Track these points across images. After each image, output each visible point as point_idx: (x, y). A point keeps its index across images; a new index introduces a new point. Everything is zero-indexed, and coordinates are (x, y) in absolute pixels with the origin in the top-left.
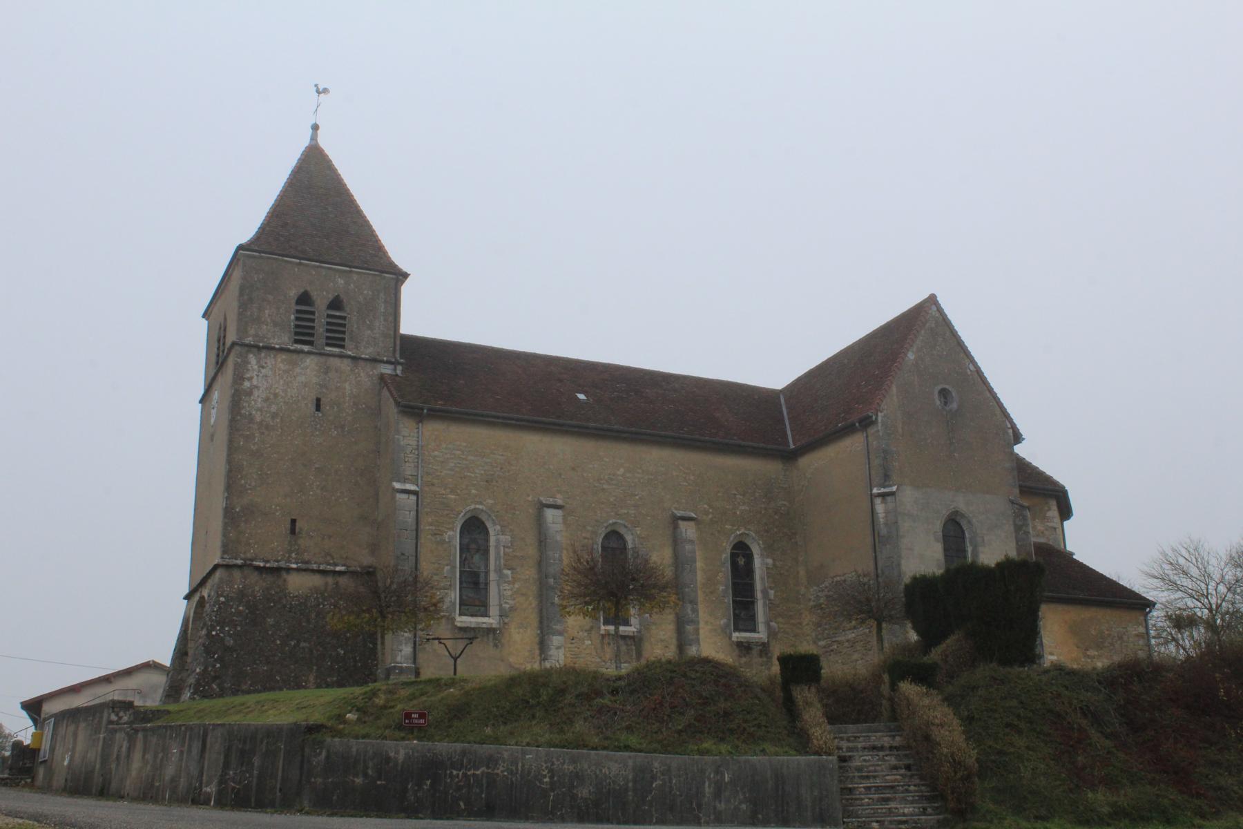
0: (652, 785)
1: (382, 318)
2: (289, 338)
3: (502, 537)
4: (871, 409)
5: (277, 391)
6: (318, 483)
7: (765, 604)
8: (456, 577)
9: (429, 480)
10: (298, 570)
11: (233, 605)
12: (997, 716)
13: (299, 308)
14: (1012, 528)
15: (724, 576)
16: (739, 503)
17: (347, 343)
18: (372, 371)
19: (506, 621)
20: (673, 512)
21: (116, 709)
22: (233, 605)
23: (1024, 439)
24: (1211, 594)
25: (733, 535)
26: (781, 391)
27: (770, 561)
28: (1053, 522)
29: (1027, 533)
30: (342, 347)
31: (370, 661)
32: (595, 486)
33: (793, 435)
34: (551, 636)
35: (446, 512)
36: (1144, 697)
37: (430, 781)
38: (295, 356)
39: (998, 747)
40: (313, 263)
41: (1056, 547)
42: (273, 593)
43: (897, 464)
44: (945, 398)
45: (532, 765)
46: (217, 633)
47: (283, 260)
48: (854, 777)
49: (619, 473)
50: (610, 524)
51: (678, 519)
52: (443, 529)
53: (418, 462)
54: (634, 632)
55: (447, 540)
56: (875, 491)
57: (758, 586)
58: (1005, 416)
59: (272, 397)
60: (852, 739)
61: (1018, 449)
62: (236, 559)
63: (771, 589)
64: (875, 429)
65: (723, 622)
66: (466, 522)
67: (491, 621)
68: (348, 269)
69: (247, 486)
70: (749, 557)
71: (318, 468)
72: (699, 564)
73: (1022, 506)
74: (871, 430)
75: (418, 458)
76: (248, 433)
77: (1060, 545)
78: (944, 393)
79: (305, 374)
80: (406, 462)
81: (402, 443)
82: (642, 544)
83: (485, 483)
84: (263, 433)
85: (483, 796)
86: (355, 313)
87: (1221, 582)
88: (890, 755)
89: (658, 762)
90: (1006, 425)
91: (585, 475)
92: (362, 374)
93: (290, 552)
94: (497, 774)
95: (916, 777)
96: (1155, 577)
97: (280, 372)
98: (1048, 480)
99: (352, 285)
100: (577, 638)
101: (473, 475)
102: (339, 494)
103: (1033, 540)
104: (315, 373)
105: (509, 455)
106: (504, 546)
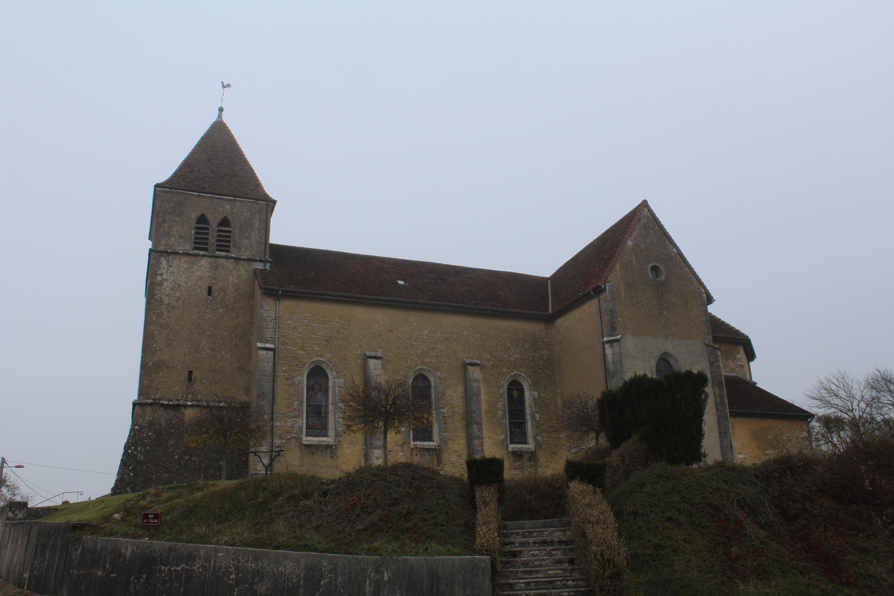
0: (320, 582)
2: (190, 246)
3: (337, 380)
5: (181, 282)
6: (208, 346)
7: (533, 424)
8: (303, 409)
11: (144, 432)
14: (708, 364)
15: (503, 405)
16: (513, 354)
17: (232, 249)
20: (464, 361)
21: (12, 509)
22: (144, 432)
23: (714, 300)
24: (856, 410)
26: (549, 278)
27: (536, 393)
28: (741, 361)
29: (719, 367)
30: (228, 251)
31: (243, 470)
35: (296, 363)
37: (145, 575)
38: (193, 258)
39: (656, 541)
41: (744, 378)
43: (621, 319)
44: (656, 272)
45: (221, 562)
46: (132, 452)
47: (187, 194)
48: (518, 572)
49: (423, 333)
50: (417, 370)
53: (275, 328)
54: (435, 446)
55: (296, 383)
56: (605, 339)
57: (528, 411)
58: (700, 284)
60: (527, 534)
61: (711, 309)
62: (148, 399)
63: (537, 413)
64: (605, 295)
66: (311, 370)
67: (329, 440)
68: (232, 198)
69: (157, 348)
70: (521, 391)
71: (209, 335)
72: (483, 397)
73: (715, 348)
74: (602, 296)
77: (746, 378)
78: (655, 269)
85: (182, 590)
87: (862, 400)
88: (557, 549)
89: (326, 561)
94: (194, 570)
95: (576, 572)
96: (816, 399)
98: (737, 332)
99: (236, 209)
101: (316, 337)
102: (223, 353)
103: (723, 374)
104: (207, 269)
105: (343, 322)
106: (338, 386)
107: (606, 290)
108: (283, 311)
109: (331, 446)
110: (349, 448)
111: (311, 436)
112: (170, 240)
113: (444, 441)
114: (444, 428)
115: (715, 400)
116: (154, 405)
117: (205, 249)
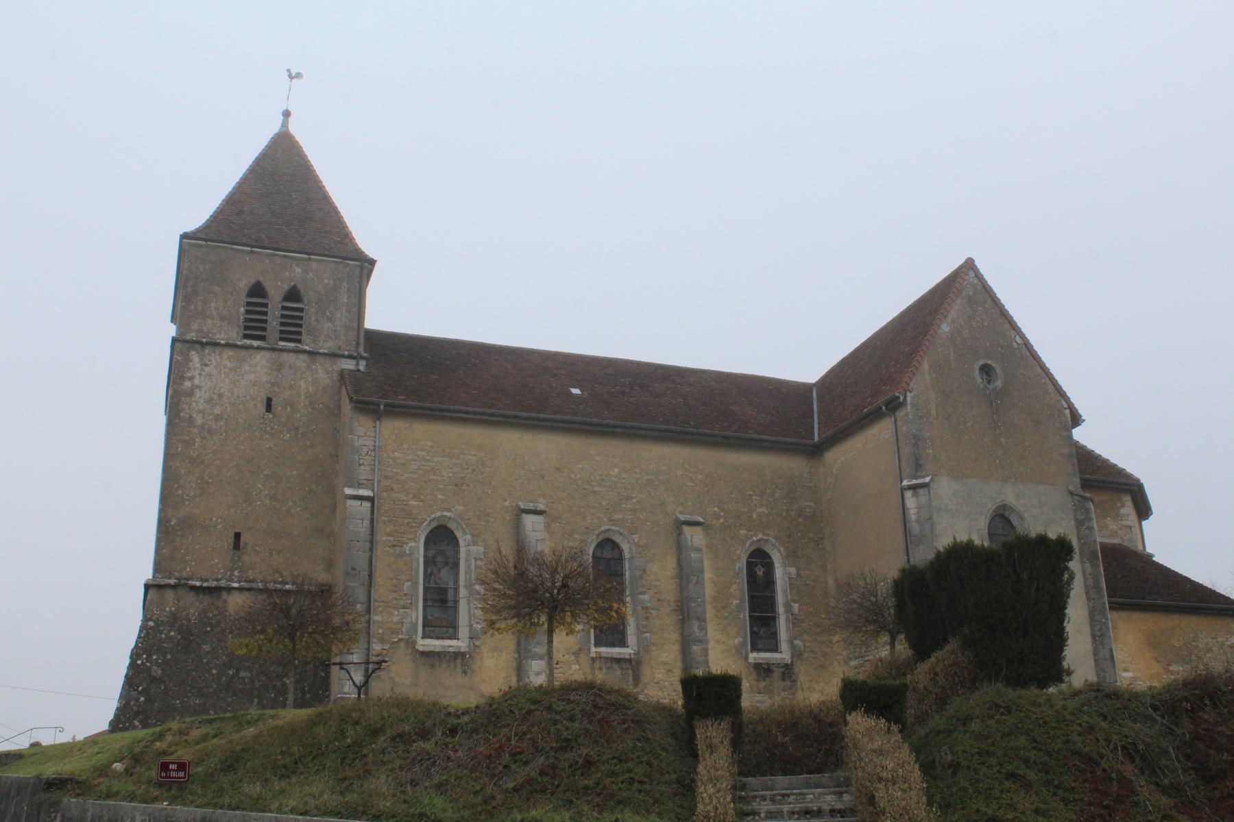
1: (344, 309)
2: (238, 333)
3: (473, 548)
4: (898, 389)
5: (222, 391)
6: (266, 492)
7: (787, 620)
8: (417, 595)
9: (387, 484)
10: (240, 589)
12: (993, 761)
13: (250, 300)
14: (1073, 523)
15: (739, 590)
17: (304, 337)
18: (332, 366)
19: (477, 643)
20: (676, 516)
23: (1084, 421)
25: (749, 541)
26: (814, 385)
27: (793, 570)
30: (299, 341)
32: (585, 489)
33: (819, 428)
34: (530, 661)
36: (1220, 729)
38: (243, 352)
40: (267, 251)
41: (1132, 548)
42: (211, 615)
46: (142, 663)
47: (232, 249)
49: (612, 473)
51: (682, 524)
52: (404, 539)
53: (374, 465)
54: (630, 654)
55: (408, 552)
56: (905, 483)
57: (780, 598)
58: (1061, 395)
59: (216, 397)
61: (1078, 434)
62: (170, 578)
65: (738, 640)
66: (432, 531)
68: (305, 256)
69: (185, 496)
70: (769, 566)
71: (267, 475)
72: (708, 575)
73: (1085, 498)
74: (900, 414)
75: (374, 460)
76: (187, 438)
78: (986, 370)
79: (253, 372)
80: (360, 465)
81: (356, 444)
82: (640, 554)
83: (455, 487)
84: (204, 438)
86: (314, 304)
90: (1063, 406)
91: (572, 476)
92: (320, 371)
93: (232, 570)
97: (226, 370)
98: (1121, 473)
99: (311, 274)
100: (562, 662)
101: (440, 479)
103: (1099, 540)
106: (475, 558)
107: (906, 405)
108: (387, 437)
109: (463, 654)
110: (492, 657)
111: (430, 637)
112: (205, 324)
113: (644, 646)
114: (645, 626)
115: (1085, 582)
116: (179, 587)
117: (262, 338)
